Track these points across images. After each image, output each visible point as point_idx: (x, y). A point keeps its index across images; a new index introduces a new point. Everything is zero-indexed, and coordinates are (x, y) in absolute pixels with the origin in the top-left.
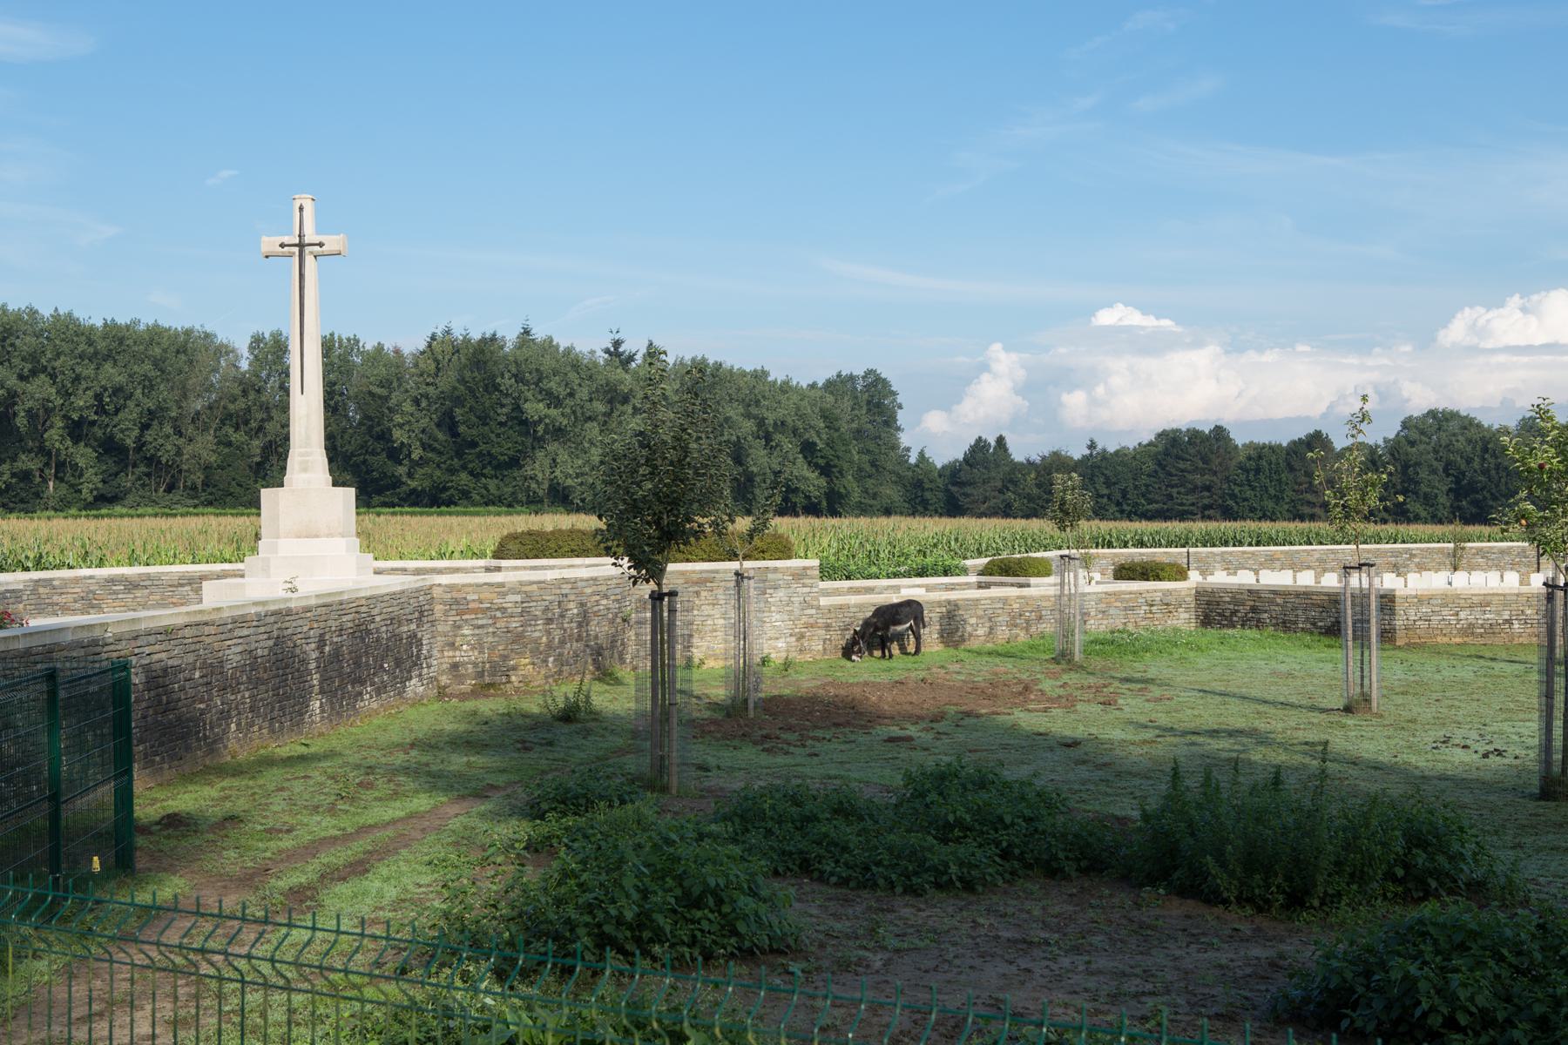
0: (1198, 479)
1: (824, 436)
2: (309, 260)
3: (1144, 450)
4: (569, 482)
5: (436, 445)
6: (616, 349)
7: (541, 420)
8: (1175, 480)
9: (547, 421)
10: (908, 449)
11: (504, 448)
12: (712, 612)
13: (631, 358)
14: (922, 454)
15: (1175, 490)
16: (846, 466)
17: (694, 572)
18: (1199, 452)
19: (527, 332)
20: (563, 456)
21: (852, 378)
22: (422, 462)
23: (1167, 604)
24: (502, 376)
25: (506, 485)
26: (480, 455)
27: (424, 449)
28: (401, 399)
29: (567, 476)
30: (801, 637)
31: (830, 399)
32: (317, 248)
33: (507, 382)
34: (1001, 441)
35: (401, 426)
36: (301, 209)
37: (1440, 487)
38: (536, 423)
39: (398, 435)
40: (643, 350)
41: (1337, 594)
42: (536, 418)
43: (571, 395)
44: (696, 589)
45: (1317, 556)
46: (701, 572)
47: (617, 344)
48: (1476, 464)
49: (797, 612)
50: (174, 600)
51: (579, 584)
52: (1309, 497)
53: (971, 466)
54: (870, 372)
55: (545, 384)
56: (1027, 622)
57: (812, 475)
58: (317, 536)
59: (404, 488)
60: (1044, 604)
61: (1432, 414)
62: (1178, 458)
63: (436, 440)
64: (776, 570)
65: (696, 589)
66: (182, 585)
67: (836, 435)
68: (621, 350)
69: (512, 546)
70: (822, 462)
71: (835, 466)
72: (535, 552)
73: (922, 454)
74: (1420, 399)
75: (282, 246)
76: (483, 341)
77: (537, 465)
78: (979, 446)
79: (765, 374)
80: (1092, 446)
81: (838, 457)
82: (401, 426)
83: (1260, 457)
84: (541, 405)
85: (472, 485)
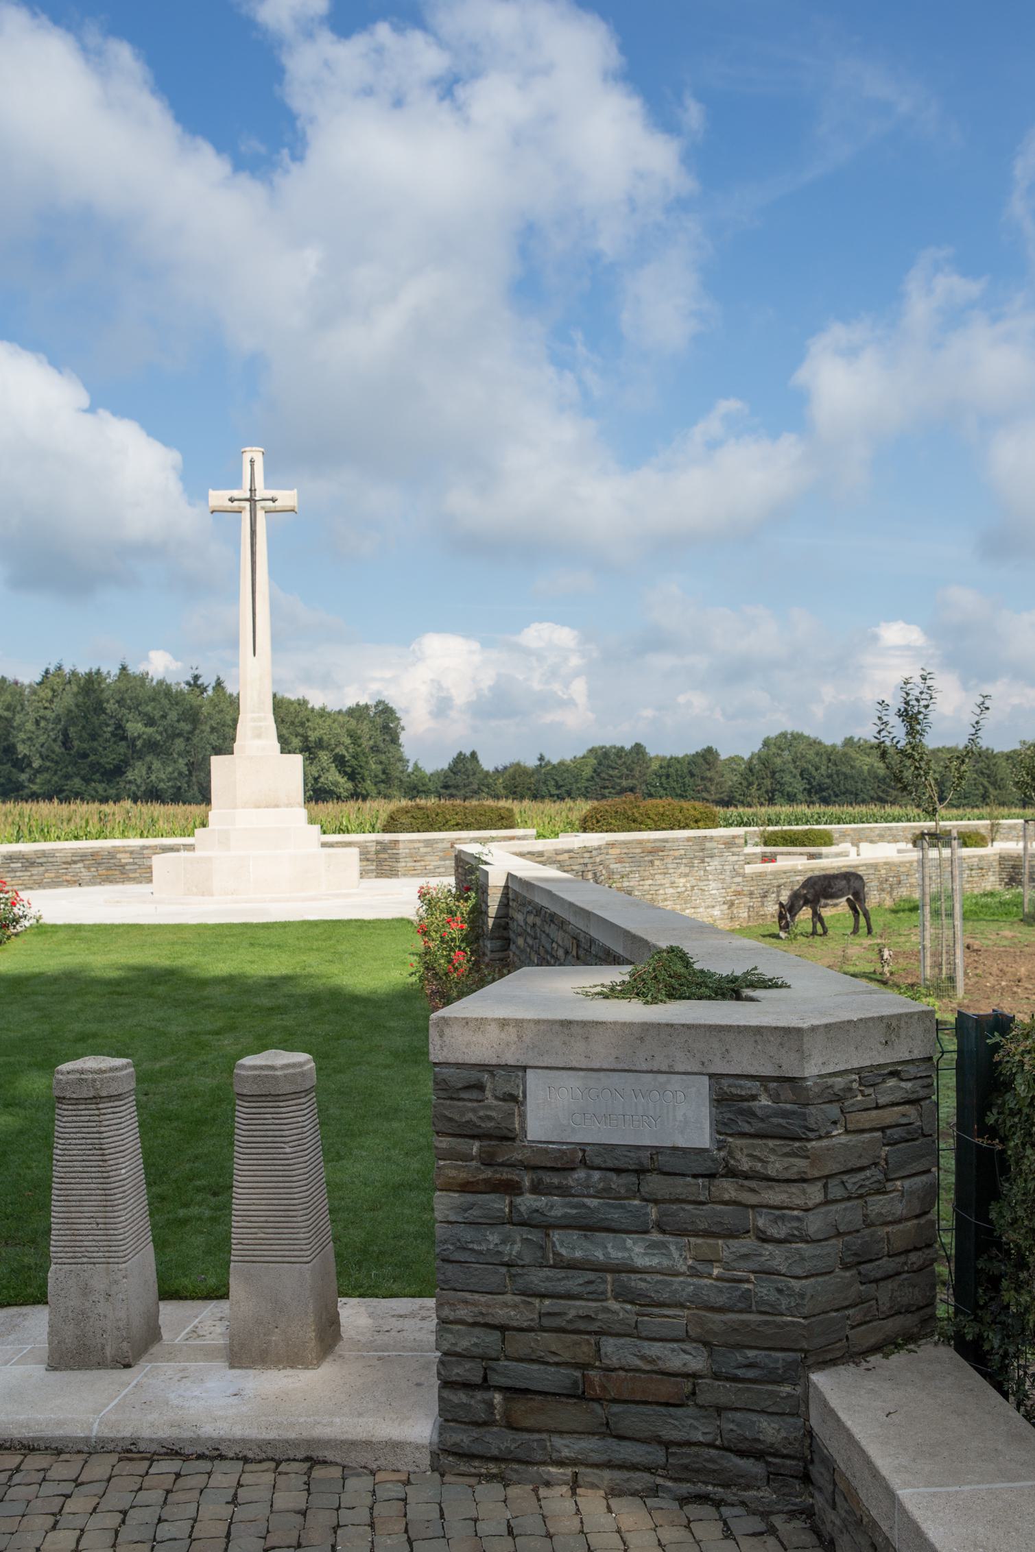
0: (624, 783)
1: (351, 750)
2: (261, 516)
3: (580, 762)
4: (162, 785)
5: (53, 756)
6: (195, 682)
7: (139, 737)
8: (607, 783)
9: (145, 736)
10: (408, 761)
11: (109, 760)
12: (663, 882)
13: (205, 690)
14: (416, 764)
15: (607, 791)
16: (366, 773)
17: (648, 841)
18: (624, 763)
19: (124, 668)
20: (156, 765)
21: (367, 707)
22: (38, 771)
23: (982, 869)
24: (108, 701)
25: (112, 788)
26: (92, 765)
27: (43, 759)
28: (23, 719)
29: (161, 780)
30: (732, 904)
31: (353, 722)
32: (270, 504)
33: (111, 706)
34: (473, 754)
35: (23, 742)
36: (252, 462)
37: (798, 786)
38: (134, 740)
39: (22, 749)
40: (213, 684)
41: (1019, 857)
42: (136, 734)
43: (164, 717)
44: (651, 858)
45: (877, 832)
46: (655, 841)
47: (196, 678)
48: (823, 770)
49: (728, 880)
50: (68, 878)
51: (594, 853)
52: (705, 795)
53: (454, 773)
54: (380, 703)
55: (143, 708)
56: (891, 885)
57: (342, 780)
58: (277, 806)
59: (27, 791)
60: (902, 869)
61: (783, 735)
62: (609, 767)
63: (53, 752)
64: (712, 838)
65: (651, 858)
66: (75, 862)
67: (359, 749)
68: (199, 682)
69: (405, 820)
70: (348, 770)
71: (359, 774)
72: (426, 826)
73: (416, 764)
74: (779, 723)
75: (232, 500)
76: (90, 674)
77: (136, 772)
78: (460, 758)
79: (305, 702)
80: (541, 758)
81: (361, 767)
82: (23, 742)
83: (669, 766)
84: (140, 725)
85: (84, 788)
